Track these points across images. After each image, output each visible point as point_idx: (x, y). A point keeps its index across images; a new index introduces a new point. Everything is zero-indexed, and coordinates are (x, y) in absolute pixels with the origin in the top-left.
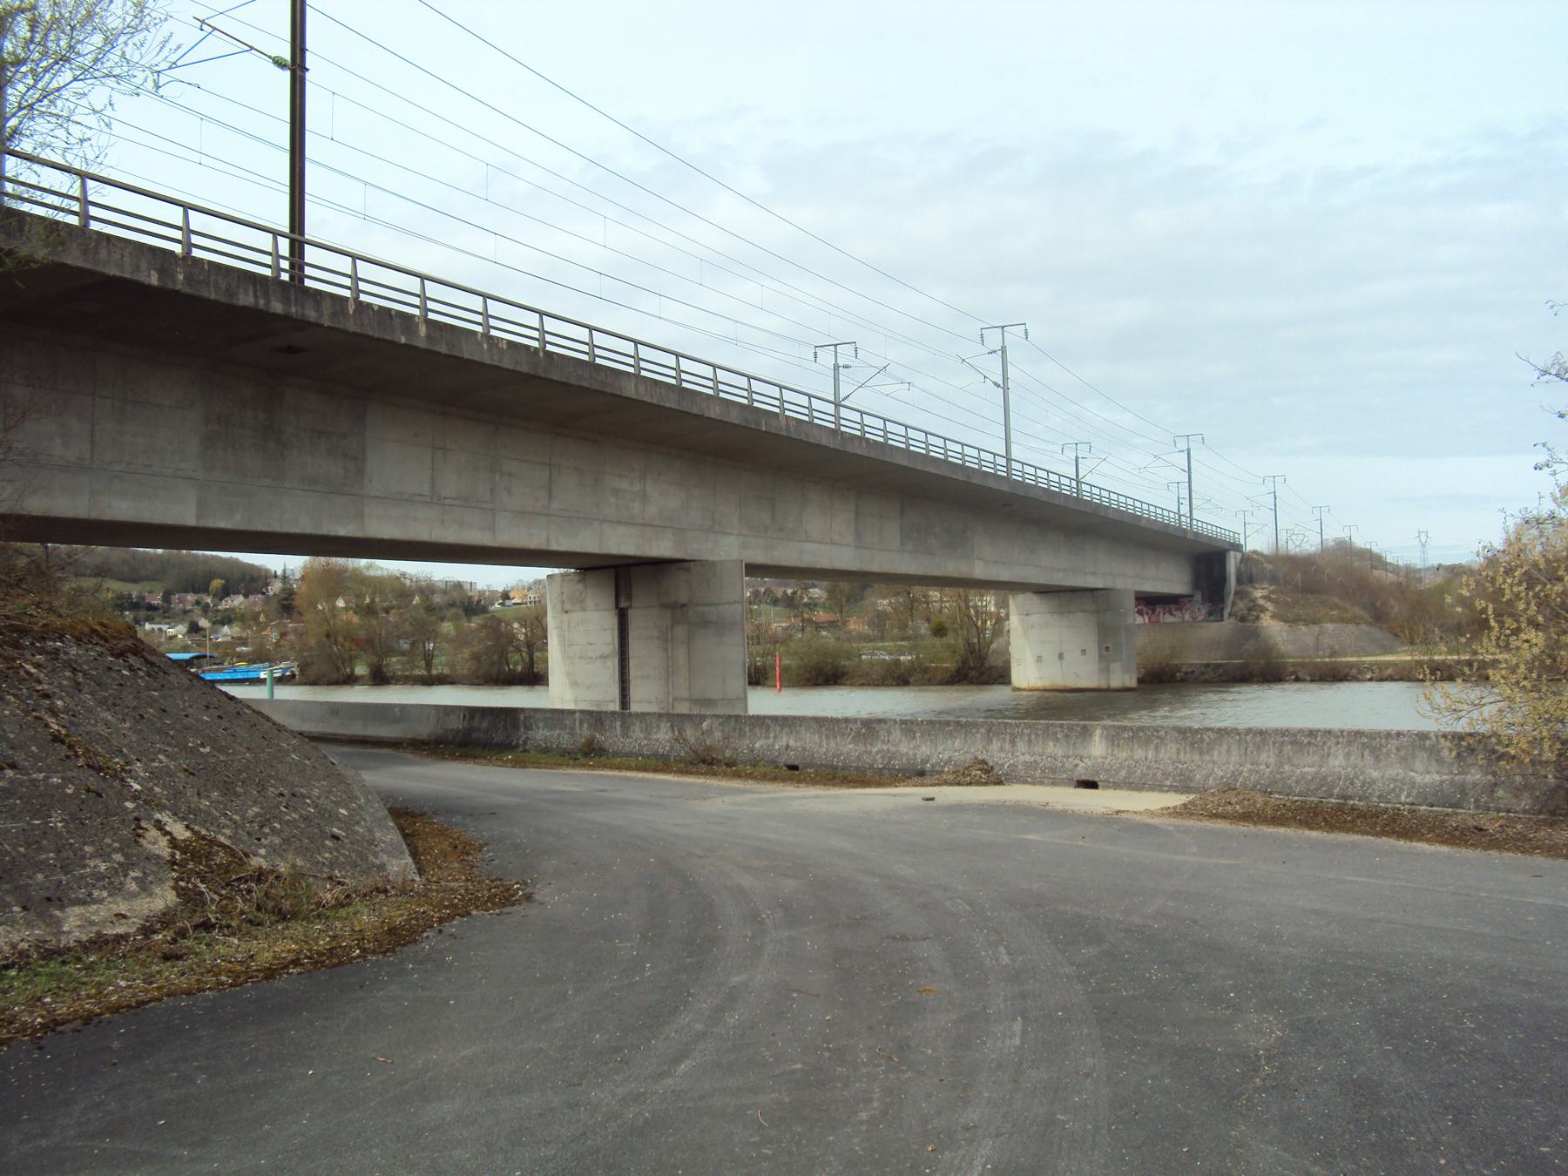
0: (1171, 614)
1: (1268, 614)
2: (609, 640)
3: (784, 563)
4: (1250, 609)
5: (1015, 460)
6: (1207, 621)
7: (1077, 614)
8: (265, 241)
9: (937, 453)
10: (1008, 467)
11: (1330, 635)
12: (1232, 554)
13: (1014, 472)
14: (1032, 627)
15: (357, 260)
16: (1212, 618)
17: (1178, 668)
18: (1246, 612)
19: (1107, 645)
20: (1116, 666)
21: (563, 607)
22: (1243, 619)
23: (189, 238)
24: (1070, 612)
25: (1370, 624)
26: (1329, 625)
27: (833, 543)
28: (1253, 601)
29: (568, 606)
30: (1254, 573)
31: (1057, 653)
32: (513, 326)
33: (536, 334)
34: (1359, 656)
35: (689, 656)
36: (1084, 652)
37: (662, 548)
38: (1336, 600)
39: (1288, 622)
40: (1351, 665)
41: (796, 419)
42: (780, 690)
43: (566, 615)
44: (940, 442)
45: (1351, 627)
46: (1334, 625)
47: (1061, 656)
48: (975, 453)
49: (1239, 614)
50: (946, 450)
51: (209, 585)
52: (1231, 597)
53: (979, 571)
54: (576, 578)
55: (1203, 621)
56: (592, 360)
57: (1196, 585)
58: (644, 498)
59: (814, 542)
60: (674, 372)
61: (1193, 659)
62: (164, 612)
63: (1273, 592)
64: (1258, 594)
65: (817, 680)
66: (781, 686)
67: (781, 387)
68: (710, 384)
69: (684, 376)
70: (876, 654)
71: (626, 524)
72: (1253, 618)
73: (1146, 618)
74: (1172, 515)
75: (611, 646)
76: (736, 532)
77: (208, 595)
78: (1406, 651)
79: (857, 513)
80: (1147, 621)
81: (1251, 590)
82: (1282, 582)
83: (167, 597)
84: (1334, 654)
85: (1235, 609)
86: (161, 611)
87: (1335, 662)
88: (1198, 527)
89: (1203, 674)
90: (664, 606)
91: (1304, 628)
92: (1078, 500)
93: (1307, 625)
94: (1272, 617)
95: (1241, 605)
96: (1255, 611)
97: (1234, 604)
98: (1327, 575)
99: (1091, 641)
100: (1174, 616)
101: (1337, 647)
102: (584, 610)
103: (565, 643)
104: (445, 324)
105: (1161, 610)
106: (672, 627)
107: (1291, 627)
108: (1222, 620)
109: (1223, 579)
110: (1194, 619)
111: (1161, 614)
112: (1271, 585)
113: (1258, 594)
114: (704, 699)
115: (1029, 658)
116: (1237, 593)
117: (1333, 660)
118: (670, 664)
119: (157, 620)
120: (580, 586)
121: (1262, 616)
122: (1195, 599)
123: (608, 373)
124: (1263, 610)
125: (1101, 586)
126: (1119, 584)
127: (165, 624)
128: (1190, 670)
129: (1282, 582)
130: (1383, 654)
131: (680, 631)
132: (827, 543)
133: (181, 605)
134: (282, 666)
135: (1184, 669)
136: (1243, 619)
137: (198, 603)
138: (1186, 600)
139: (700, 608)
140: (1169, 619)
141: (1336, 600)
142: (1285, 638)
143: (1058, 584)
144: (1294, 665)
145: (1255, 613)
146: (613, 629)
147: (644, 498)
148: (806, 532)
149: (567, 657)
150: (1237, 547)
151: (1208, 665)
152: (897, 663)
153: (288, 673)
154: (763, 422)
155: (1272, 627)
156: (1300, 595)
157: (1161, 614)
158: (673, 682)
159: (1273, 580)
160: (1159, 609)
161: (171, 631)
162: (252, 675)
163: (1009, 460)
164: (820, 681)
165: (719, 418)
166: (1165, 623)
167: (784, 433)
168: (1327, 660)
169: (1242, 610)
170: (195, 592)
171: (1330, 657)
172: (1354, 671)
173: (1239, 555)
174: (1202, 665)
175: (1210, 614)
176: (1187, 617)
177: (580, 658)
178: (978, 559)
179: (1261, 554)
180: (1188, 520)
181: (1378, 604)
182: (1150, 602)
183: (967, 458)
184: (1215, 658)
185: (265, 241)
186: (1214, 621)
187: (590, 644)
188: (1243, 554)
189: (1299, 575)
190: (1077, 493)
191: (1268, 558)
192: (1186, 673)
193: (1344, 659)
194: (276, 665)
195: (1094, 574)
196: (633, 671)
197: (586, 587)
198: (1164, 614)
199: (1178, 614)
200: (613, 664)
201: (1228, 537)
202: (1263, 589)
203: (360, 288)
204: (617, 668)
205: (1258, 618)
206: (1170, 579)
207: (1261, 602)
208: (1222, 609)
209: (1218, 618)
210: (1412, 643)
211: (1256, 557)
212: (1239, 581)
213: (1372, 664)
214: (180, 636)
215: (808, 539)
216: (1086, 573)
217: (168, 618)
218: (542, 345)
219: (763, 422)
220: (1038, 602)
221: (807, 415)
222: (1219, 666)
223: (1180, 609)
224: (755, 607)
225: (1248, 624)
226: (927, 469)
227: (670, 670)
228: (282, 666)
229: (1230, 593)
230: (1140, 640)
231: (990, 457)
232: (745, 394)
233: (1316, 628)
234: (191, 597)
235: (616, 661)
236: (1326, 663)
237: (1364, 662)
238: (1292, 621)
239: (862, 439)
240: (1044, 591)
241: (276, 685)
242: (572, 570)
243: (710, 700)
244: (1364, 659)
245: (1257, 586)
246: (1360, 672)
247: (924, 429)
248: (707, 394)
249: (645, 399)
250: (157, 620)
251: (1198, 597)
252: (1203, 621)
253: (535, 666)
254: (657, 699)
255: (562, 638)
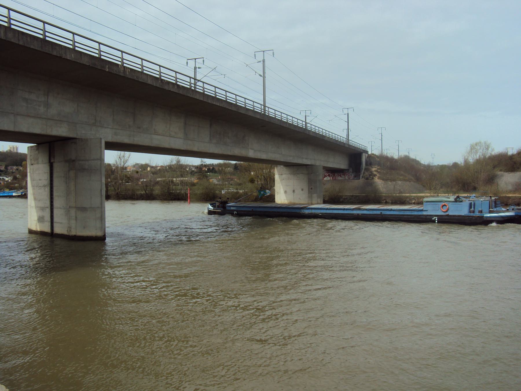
0: (341, 176)
1: (377, 177)
2: (46, 176)
3: (141, 144)
4: (370, 175)
5: (267, 107)
6: (354, 179)
7: (300, 175)
8: (188, 79)
9: (249, 107)
10: (306, 125)
11: (400, 186)
12: (364, 154)
13: (308, 127)
14: (283, 179)
15: (45, 24)
16: (356, 178)
17: (341, 197)
18: (368, 176)
19: (312, 187)
20: (315, 195)
21: (31, 162)
22: (367, 179)
23: (75, 44)
24: (297, 174)
25: (414, 182)
26: (399, 182)
27: (170, 136)
28: (371, 172)
29: (33, 162)
30: (372, 161)
31: (292, 190)
32: (151, 70)
33: (41, 32)
34: (410, 194)
35: (75, 187)
36: (302, 190)
37: (61, 131)
38: (402, 172)
39: (384, 180)
40: (407, 197)
41: (131, 68)
42: (190, 203)
43: (32, 166)
44: (280, 114)
45: (408, 183)
46: (401, 182)
47: (294, 191)
48: (291, 118)
49: (366, 177)
50: (227, 96)
51: (22, 163)
52: (363, 170)
53: (251, 154)
54: (35, 148)
55: (352, 179)
56: (9, 26)
57: (350, 165)
58: (47, 105)
59: (159, 135)
60: (140, 66)
61: (347, 193)
62: (5, 172)
63: (378, 169)
64: (374, 169)
65: (207, 199)
66: (190, 201)
67: (176, 72)
68: (214, 93)
69: (247, 105)
70: (229, 189)
71: (34, 117)
72: (371, 178)
73: (331, 178)
74: (344, 139)
75: (47, 181)
76: (111, 127)
77: (21, 167)
78: (428, 192)
79: (185, 124)
80: (331, 179)
81: (371, 168)
82: (382, 165)
83: (6, 167)
84: (401, 192)
85: (364, 175)
86: (4, 172)
87: (401, 196)
88: (271, 113)
89: (350, 199)
90: (66, 161)
91: (390, 183)
92: (306, 129)
93: (391, 181)
94: (378, 178)
95: (367, 173)
96: (372, 176)
97: (364, 173)
98: (400, 163)
99: (305, 186)
100: (342, 177)
101: (402, 190)
102: (38, 164)
103: (32, 180)
104: (16, 30)
105: (337, 175)
106: (69, 171)
107: (385, 182)
108: (359, 179)
109: (360, 163)
110: (349, 178)
111: (337, 176)
112: (378, 166)
113: (374, 169)
114: (82, 207)
115: (282, 191)
116: (365, 169)
117: (400, 195)
118: (68, 190)
119: (2, 175)
120: (37, 152)
121: (374, 178)
122: (349, 171)
123: (82, 54)
124: (375, 175)
125: (309, 163)
126: (318, 163)
127: (5, 176)
128: (346, 197)
129: (382, 165)
130: (419, 193)
131: (72, 173)
132: (167, 136)
133: (11, 170)
134: (21, 191)
135: (343, 197)
136: (367, 179)
137: (17, 169)
138: (346, 171)
139: (80, 162)
140: (340, 178)
141: (402, 172)
142: (383, 186)
143: (290, 161)
144: (385, 196)
145: (372, 177)
146: (48, 173)
147: (47, 105)
148: (155, 129)
149: (33, 186)
150: (366, 152)
151: (352, 196)
152: (238, 193)
153: (23, 194)
154: (107, 67)
155: (378, 182)
156: (389, 170)
157: (337, 176)
158: (69, 198)
159: (379, 164)
160: (336, 174)
161: (7, 179)
162: (10, 194)
163: (265, 106)
164: (208, 199)
165: (74, 60)
166: (339, 180)
167: (122, 75)
168: (398, 195)
169: (367, 175)
170: (17, 166)
171: (399, 194)
172: (408, 199)
173: (367, 155)
174: (350, 196)
175: (355, 177)
176: (346, 178)
177: (37, 186)
178: (251, 149)
179: (375, 155)
180: (263, 107)
181: (418, 175)
182: (333, 172)
183: (283, 118)
184: (356, 193)
185: (259, 106)
186: (357, 179)
187: (40, 180)
188: (368, 155)
189: (389, 163)
190: (306, 127)
191: (377, 157)
192: (344, 199)
193: (404, 195)
194: (19, 190)
195: (306, 159)
196: (55, 194)
197: (39, 153)
198: (338, 176)
199: (343, 176)
200: (48, 189)
201: (363, 148)
202: (375, 168)
203: (124, 62)
204: (49, 192)
205: (373, 178)
206: (340, 163)
207: (375, 173)
208: (360, 175)
209: (358, 178)
210: (430, 189)
211: (373, 156)
212: (366, 164)
213: (414, 197)
214: (10, 181)
215: (156, 133)
216: (303, 158)
217: (7, 174)
218: (122, 64)
219: (107, 67)
220: (286, 170)
221: (140, 69)
222: (357, 196)
223: (344, 175)
224: (209, 173)
225: (369, 181)
226: (215, 103)
227: (68, 193)
228: (21, 191)
229: (363, 169)
230: (328, 186)
231: (301, 122)
232: (71, 43)
233: (394, 183)
234: (15, 168)
235: (49, 188)
236: (397, 196)
237: (412, 196)
238: (385, 180)
239: (275, 118)
240: (288, 165)
241: (274, 201)
242: (35, 145)
243: (84, 208)
244: (412, 195)
245: (373, 166)
246: (411, 200)
247: (225, 89)
248: (200, 92)
249: (13, 41)
250: (2, 175)
251: (351, 170)
252: (352, 179)
253: (109, 192)
254: (63, 207)
255: (31, 176)
